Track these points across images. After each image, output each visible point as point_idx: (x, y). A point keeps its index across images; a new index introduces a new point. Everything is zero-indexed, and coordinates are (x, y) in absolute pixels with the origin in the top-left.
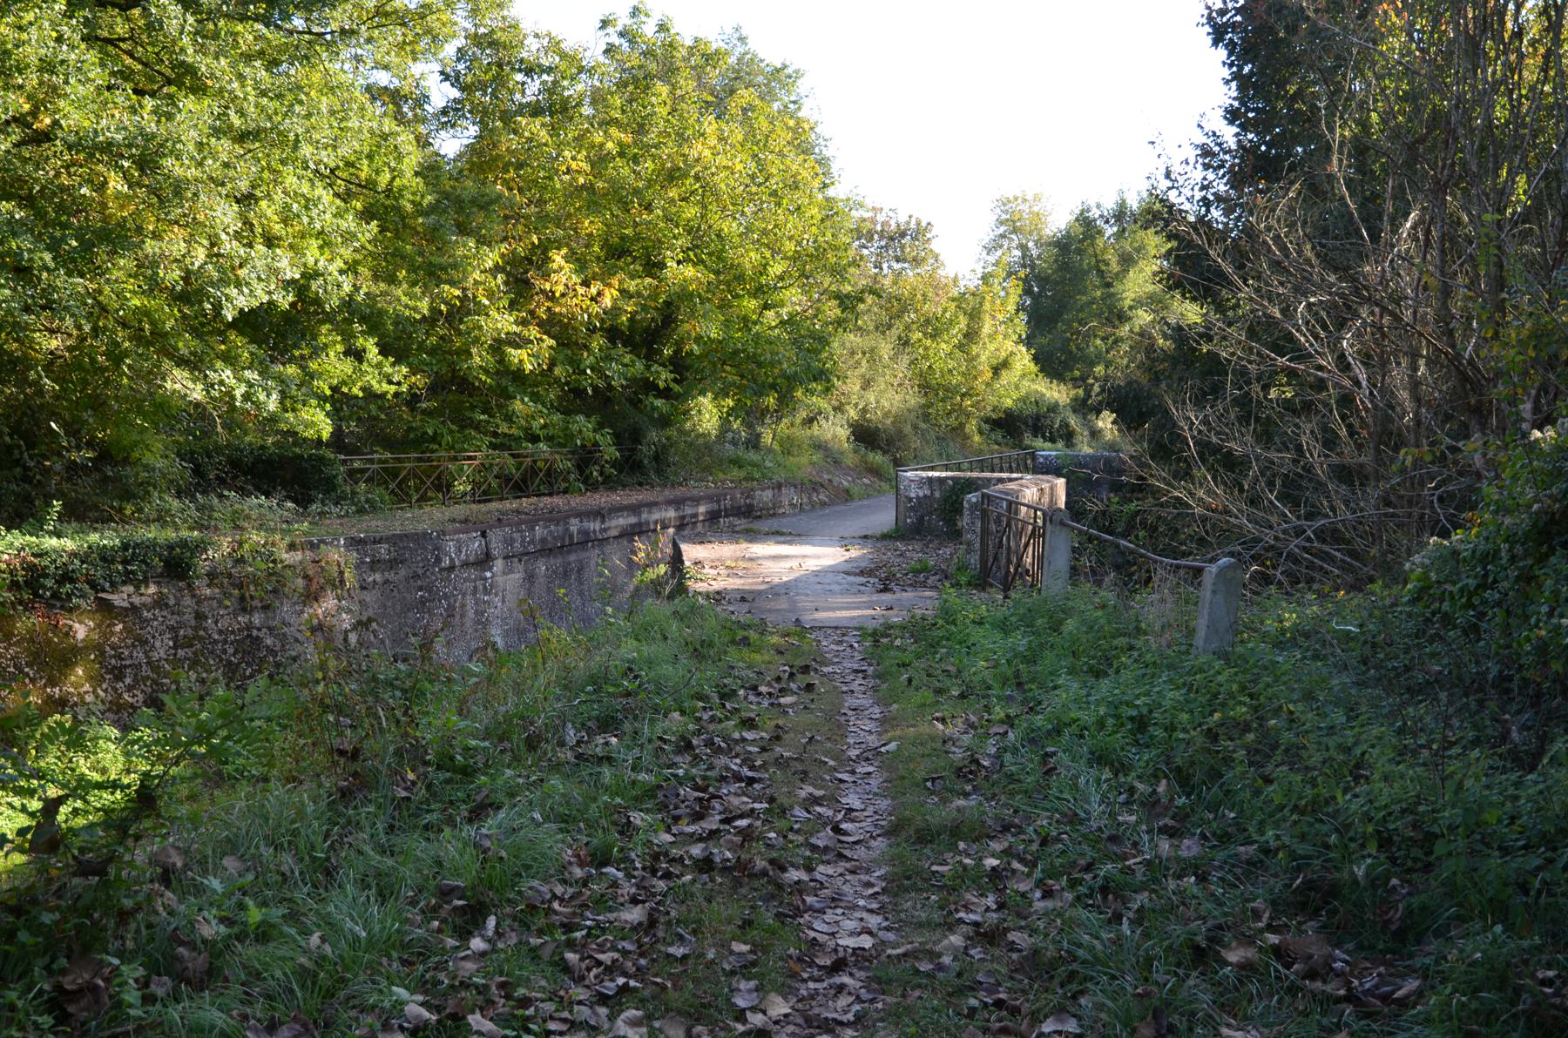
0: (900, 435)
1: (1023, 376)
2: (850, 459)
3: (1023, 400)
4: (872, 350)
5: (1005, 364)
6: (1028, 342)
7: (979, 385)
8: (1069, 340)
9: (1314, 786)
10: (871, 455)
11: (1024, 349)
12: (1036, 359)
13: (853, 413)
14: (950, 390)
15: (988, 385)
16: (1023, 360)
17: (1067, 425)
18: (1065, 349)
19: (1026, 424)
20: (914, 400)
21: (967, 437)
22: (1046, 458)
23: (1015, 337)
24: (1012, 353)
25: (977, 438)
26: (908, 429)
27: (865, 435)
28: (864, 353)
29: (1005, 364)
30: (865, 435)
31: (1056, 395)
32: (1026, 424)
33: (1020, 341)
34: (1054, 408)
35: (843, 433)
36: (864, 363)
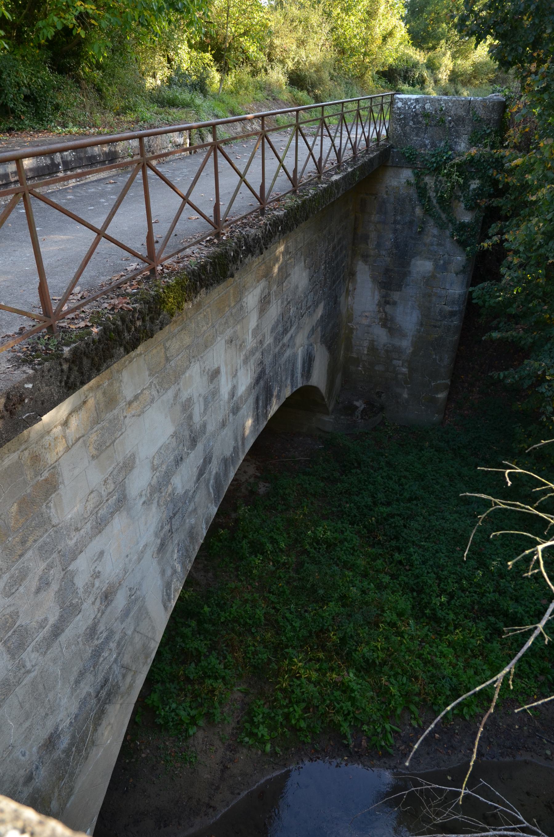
0: (321, 81)
1: (401, 44)
2: (285, 96)
3: (399, 59)
4: (306, 19)
5: (390, 34)
6: (406, 19)
7: (374, 47)
8: (428, 25)
9: (327, 706)
10: (300, 94)
11: (403, 24)
12: (409, 32)
13: (290, 65)
14: (354, 51)
15: (380, 48)
16: (402, 32)
17: (422, 76)
18: (425, 30)
19: (400, 75)
20: (331, 55)
21: (365, 83)
22: (405, 102)
23: (398, 16)
24: (395, 27)
25: (371, 83)
26: (326, 76)
27: (297, 80)
28: (300, 22)
29: (390, 34)
30: (297, 80)
31: (418, 58)
32: (400, 75)
33: (402, 18)
34: (415, 65)
35: (283, 79)
36: (301, 29)
